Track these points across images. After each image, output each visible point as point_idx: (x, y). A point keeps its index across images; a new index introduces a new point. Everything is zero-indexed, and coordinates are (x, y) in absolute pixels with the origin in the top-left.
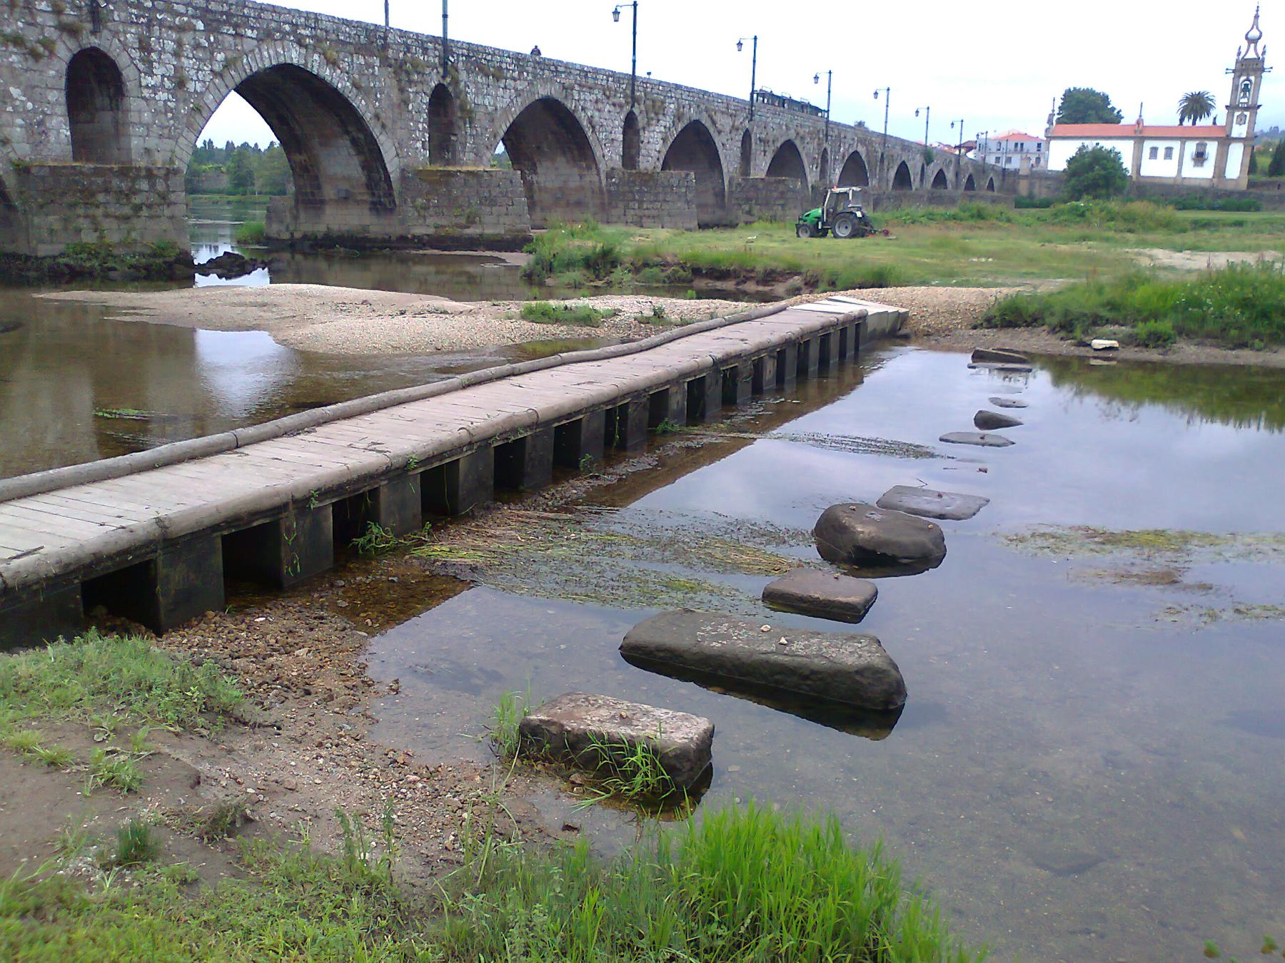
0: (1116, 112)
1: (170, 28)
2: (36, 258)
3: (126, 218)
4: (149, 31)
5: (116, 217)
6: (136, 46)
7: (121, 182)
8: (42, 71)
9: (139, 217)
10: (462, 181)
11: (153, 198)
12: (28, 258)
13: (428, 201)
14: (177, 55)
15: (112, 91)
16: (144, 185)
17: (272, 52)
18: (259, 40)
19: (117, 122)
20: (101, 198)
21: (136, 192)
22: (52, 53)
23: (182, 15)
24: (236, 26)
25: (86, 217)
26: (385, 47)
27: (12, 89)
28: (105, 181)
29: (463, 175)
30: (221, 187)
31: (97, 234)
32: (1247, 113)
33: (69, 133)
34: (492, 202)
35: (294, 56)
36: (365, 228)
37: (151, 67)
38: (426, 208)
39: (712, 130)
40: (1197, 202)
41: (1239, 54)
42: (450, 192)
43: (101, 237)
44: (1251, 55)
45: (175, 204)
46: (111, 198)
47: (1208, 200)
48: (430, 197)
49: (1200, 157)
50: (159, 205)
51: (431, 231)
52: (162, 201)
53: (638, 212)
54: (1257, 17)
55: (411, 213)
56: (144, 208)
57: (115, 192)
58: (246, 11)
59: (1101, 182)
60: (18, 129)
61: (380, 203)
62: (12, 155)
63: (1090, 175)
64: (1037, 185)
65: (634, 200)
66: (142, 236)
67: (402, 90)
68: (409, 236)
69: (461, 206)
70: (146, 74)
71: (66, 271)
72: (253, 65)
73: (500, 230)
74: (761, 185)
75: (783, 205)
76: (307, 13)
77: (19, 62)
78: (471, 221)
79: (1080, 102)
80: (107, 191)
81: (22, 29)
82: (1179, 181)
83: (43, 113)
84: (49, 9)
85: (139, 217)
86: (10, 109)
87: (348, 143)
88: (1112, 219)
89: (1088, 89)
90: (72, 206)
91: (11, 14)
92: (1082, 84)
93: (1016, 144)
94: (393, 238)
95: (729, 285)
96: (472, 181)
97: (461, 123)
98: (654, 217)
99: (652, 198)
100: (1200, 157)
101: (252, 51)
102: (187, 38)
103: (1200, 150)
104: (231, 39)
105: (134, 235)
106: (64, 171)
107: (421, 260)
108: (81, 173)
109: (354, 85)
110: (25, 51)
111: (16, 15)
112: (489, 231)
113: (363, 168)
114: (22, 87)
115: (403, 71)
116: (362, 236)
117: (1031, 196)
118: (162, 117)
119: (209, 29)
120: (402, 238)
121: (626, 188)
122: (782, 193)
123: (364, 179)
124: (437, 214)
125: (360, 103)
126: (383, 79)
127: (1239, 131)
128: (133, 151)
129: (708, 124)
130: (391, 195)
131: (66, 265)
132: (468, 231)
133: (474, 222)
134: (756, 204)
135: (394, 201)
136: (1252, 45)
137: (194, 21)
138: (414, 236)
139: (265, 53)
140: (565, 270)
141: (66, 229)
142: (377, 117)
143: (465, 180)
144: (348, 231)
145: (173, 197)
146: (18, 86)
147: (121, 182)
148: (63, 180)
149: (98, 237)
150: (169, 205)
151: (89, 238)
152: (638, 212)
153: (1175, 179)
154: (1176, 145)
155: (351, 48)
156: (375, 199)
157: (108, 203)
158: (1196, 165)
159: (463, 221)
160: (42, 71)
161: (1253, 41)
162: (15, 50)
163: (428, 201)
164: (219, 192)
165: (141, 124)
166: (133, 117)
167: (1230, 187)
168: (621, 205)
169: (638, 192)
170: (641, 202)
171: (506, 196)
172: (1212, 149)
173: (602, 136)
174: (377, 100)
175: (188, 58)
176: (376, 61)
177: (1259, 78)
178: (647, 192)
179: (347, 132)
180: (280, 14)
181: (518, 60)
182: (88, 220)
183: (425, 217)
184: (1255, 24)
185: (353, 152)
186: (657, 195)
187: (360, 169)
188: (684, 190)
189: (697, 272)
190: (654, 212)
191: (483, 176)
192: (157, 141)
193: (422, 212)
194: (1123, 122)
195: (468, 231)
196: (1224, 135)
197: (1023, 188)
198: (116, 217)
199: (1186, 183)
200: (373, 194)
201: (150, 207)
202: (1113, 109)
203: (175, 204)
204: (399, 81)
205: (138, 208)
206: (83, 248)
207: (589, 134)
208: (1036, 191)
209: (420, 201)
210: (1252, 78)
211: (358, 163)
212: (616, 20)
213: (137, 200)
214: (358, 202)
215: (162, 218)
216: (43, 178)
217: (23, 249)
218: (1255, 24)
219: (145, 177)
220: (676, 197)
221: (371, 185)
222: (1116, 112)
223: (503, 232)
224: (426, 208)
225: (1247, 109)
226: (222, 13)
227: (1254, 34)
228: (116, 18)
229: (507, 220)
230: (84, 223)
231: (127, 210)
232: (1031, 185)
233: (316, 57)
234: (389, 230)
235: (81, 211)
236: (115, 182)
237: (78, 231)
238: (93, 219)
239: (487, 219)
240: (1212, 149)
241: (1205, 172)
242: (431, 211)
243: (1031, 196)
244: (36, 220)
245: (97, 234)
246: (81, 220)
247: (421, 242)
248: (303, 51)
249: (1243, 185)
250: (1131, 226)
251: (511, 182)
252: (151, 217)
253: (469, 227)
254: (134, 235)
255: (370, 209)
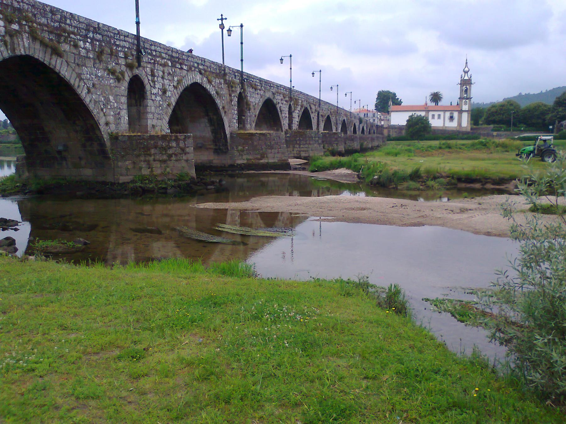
0: (399, 100)
1: (161, 65)
2: (118, 183)
3: (164, 161)
4: (154, 66)
5: (160, 161)
6: (150, 74)
7: (163, 143)
8: (120, 87)
9: (171, 160)
10: (258, 138)
11: (179, 151)
12: (113, 184)
13: (244, 147)
14: (163, 78)
15: (137, 96)
16: (174, 144)
17: (191, 77)
18: (187, 71)
19: (140, 112)
20: (153, 151)
21: (170, 148)
22: (124, 78)
23: (165, 58)
24: (181, 64)
25: (145, 161)
26: (225, 74)
27: (110, 97)
28: (155, 142)
29: (258, 135)
30: (9, 140)
31: (150, 170)
32: (467, 101)
33: (127, 118)
34: (271, 147)
35: (198, 78)
36: (211, 161)
37: (155, 84)
38: (243, 151)
39: (310, 111)
40: (456, 136)
41: (462, 77)
42: (253, 143)
43: (152, 171)
44: (466, 78)
45: (189, 153)
46: (157, 151)
47: (461, 135)
48: (244, 146)
49: (451, 118)
50: (180, 154)
51: (245, 162)
52: (182, 152)
53: (299, 149)
54: (467, 63)
55: (236, 153)
56: (173, 156)
57: (160, 148)
58: (184, 56)
59: (422, 129)
60: (112, 117)
61: (220, 149)
62: (109, 130)
63: (418, 126)
64: (391, 131)
65: (297, 144)
66: (172, 170)
67: (230, 95)
68: (236, 165)
69: (258, 150)
70: (153, 88)
71: (140, 189)
72: (186, 83)
73: (276, 160)
74: (327, 135)
75: (337, 144)
76: (202, 58)
77: (113, 83)
78: (262, 157)
79: (385, 96)
80: (156, 147)
81: (114, 66)
82: (444, 128)
83: (120, 108)
84: (123, 56)
85: (171, 160)
86: (109, 107)
87: (207, 121)
88: (497, 147)
89: (529, 94)
90: (138, 156)
91: (111, 58)
92: (385, 89)
93: (365, 114)
94: (227, 166)
95: (477, 186)
96: (262, 138)
97: (246, 110)
98: (305, 151)
99: (305, 143)
100: (451, 118)
101: (185, 76)
102: (166, 69)
103: (451, 115)
104: (178, 70)
105: (168, 170)
106: (135, 138)
107: (240, 176)
108: (144, 139)
109: (217, 93)
110: (115, 77)
111: (113, 60)
112: (271, 161)
113: (212, 133)
114: (114, 96)
115: (230, 85)
116: (209, 165)
117: (389, 136)
118: (158, 109)
119: (173, 66)
120: (232, 166)
121: (293, 139)
122: (336, 138)
123: (212, 138)
124: (247, 154)
125: (218, 101)
126: (224, 91)
127: (465, 107)
128: (149, 126)
129: (309, 109)
130: (226, 145)
131: (140, 187)
132: (261, 161)
133: (264, 157)
134: (326, 144)
135: (228, 148)
136: (466, 74)
137: (168, 61)
138: (238, 164)
139: (189, 77)
140: (403, 181)
141: (134, 168)
142: (223, 108)
143: (259, 137)
144: (201, 163)
145: (187, 150)
146: (112, 95)
147: (163, 143)
148: (134, 142)
149: (150, 171)
150: (185, 154)
151: (146, 172)
152: (299, 149)
153: (442, 127)
154: (442, 113)
155: (214, 75)
156: (217, 147)
157: (156, 154)
158: (450, 121)
159: (259, 157)
160: (120, 87)
161: (466, 72)
162: (112, 77)
163: (244, 147)
164: (9, 143)
165: (152, 113)
166: (149, 109)
167: (464, 130)
168: (291, 146)
169: (298, 140)
170: (300, 145)
171: (277, 144)
172: (456, 115)
173: (283, 116)
174: (223, 100)
175: (166, 80)
176: (222, 81)
177: (470, 87)
178: (302, 140)
179: (208, 115)
180: (194, 58)
181: (260, 81)
182: (146, 163)
183: (242, 155)
184: (466, 66)
185: (208, 125)
186: (306, 141)
187: (210, 133)
188: (317, 139)
189: (459, 180)
190: (305, 149)
191: (267, 135)
192: (156, 121)
193: (241, 153)
194: (402, 104)
195: (261, 161)
196: (460, 109)
197: (385, 132)
198: (160, 161)
199: (447, 129)
200: (216, 145)
201: (176, 155)
202: (398, 99)
203: (189, 153)
204: (229, 91)
205: (170, 156)
206: (143, 179)
207: (280, 114)
208: (391, 134)
209: (240, 148)
210: (468, 87)
211: (210, 130)
212: (282, 63)
213: (170, 152)
214: (207, 149)
215: (183, 161)
216: (124, 142)
217: (110, 178)
218: (466, 66)
219: (174, 140)
220: (314, 142)
221: (216, 140)
222: (399, 100)
223: (277, 161)
224: (243, 151)
225: (467, 99)
226: (177, 58)
227: (466, 69)
228: (144, 61)
229: (279, 155)
230: (143, 165)
231: (165, 157)
232: (389, 131)
233: (205, 78)
234: (224, 162)
235: (142, 158)
236: (160, 143)
237: (140, 169)
238: (148, 162)
239: (269, 155)
240: (456, 115)
241: (454, 125)
242: (245, 152)
243: (389, 136)
244: (120, 164)
245: (150, 170)
246: (142, 163)
247: (242, 167)
248: (201, 76)
249: (469, 129)
250: (507, 149)
251: (279, 138)
252: (176, 160)
253: (262, 159)
254: (168, 170)
255: (214, 152)
